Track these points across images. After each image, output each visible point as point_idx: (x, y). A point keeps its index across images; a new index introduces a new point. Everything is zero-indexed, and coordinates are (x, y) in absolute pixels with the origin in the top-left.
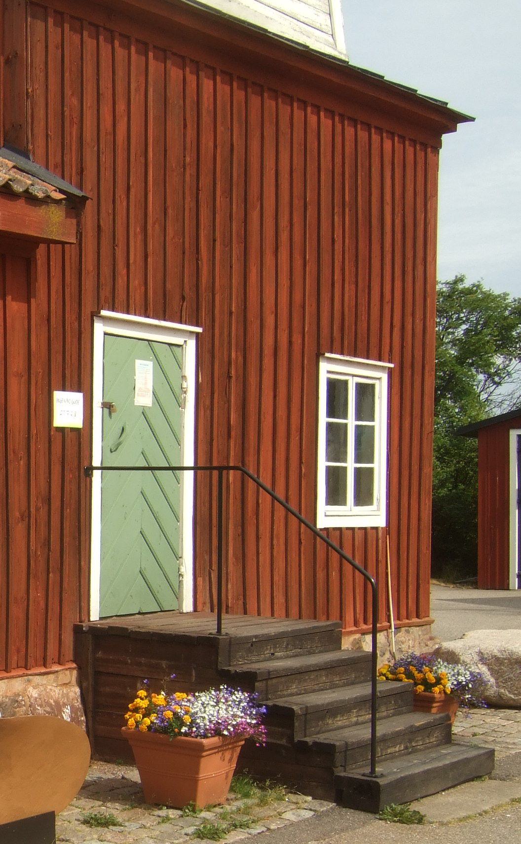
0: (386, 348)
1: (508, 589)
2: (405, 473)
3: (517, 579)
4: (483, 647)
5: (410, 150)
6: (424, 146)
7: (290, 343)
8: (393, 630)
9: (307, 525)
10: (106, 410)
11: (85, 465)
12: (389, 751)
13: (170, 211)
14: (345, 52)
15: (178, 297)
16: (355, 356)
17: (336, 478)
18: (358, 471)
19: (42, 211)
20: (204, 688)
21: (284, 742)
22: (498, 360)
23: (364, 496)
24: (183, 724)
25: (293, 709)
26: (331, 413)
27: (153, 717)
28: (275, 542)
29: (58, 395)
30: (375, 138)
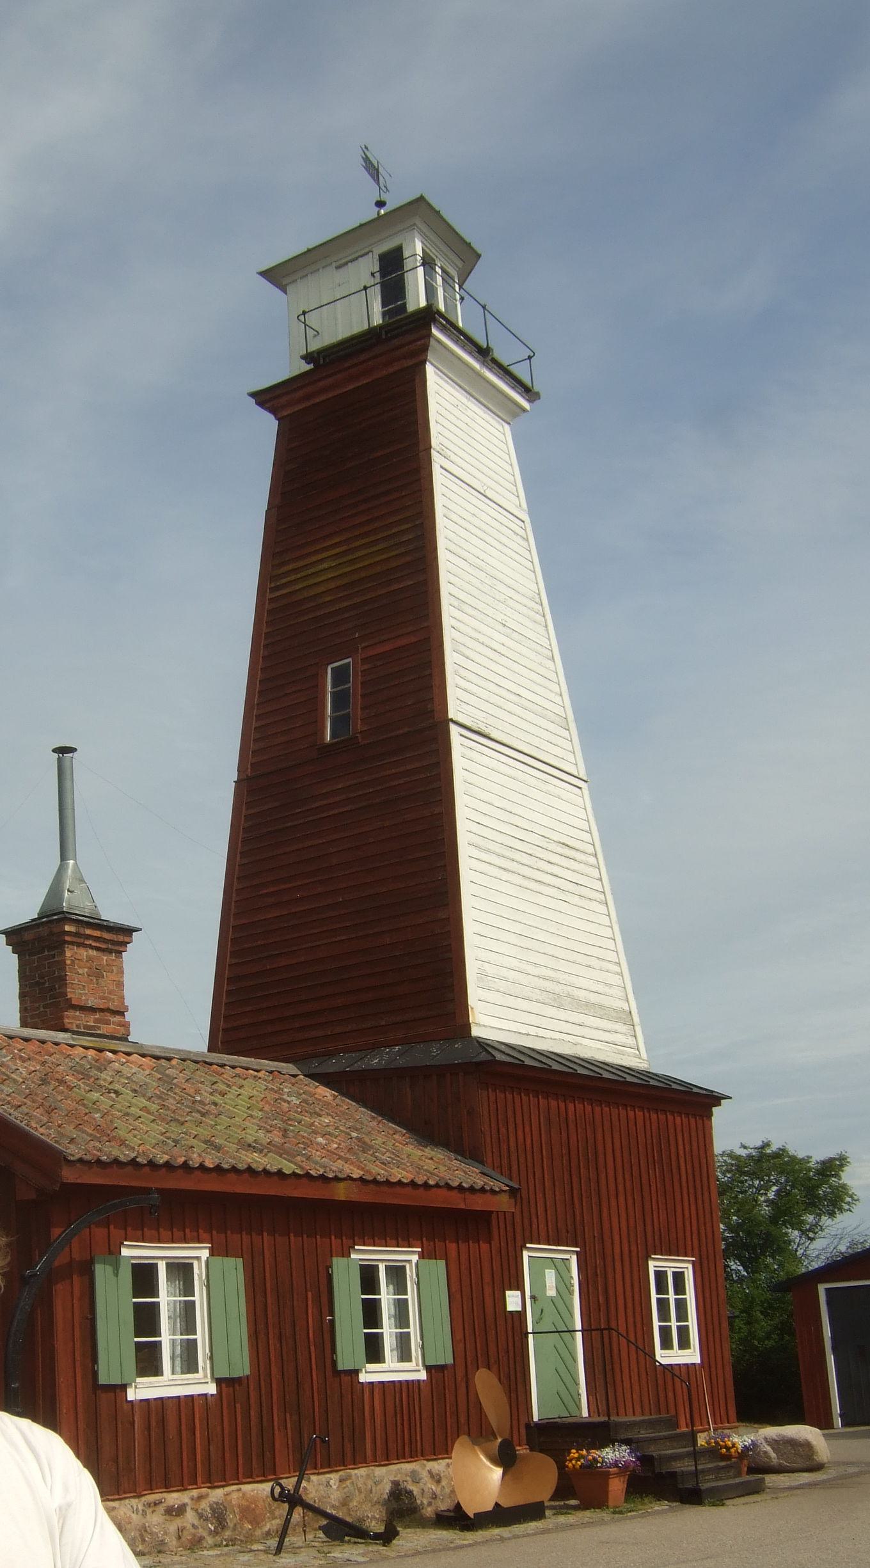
0: (689, 1248)
1: (833, 1428)
2: (710, 1327)
3: (839, 1419)
4: (766, 1434)
5: (692, 1121)
6: (702, 1117)
7: (630, 1251)
8: (712, 1430)
9: (649, 1356)
10: (533, 1300)
11: (524, 1330)
12: (707, 1478)
13: (557, 1183)
14: (646, 1059)
15: (564, 1231)
16: (670, 1255)
17: (665, 1332)
18: (679, 1327)
19: (498, 1197)
20: (607, 1446)
21: (650, 1474)
22: (810, 1218)
23: (684, 1344)
24: (598, 1462)
25: (653, 1456)
26: (658, 1292)
27: (582, 1461)
28: (632, 1373)
29: (508, 1293)
30: (670, 1117)
